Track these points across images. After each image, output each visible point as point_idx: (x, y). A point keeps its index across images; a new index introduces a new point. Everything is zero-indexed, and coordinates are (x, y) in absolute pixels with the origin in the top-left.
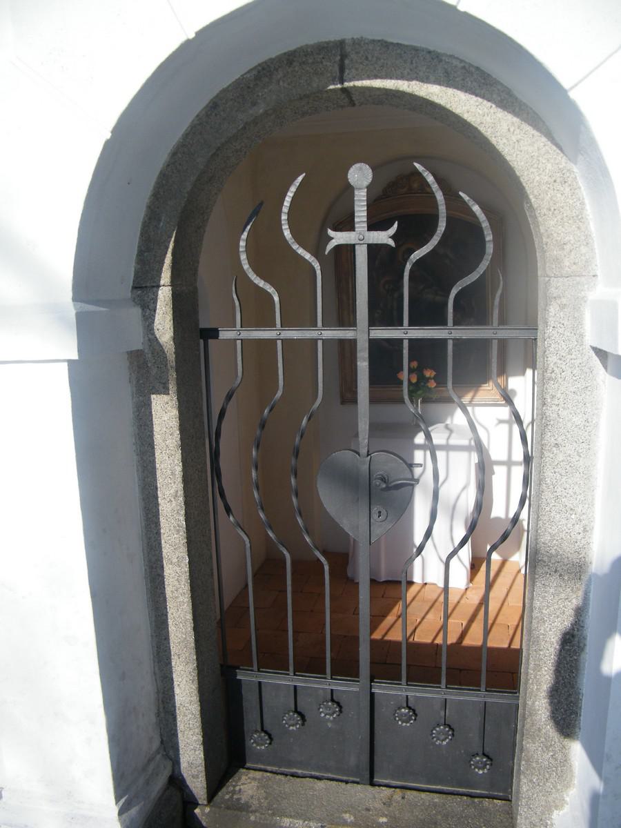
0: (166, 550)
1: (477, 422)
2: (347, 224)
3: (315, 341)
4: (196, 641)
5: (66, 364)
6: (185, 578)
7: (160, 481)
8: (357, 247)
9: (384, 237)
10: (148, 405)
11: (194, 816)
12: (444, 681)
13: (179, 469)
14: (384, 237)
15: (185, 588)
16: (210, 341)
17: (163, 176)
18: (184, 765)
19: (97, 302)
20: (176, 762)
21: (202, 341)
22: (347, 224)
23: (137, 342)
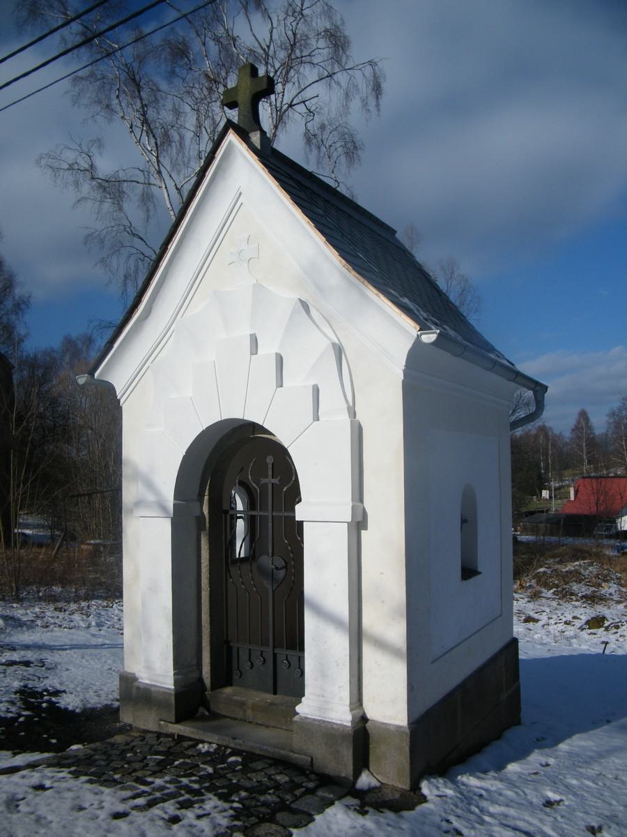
0: (203, 585)
1: (295, 188)
2: (266, 477)
3: (282, 516)
4: (210, 621)
5: (346, 524)
6: (208, 595)
7: (202, 561)
8: (304, 523)
9: (275, 481)
10: (200, 534)
11: (205, 695)
12: (298, 648)
13: (208, 557)
14: (275, 481)
15: (208, 600)
16: (363, 532)
17: (207, 461)
18: (204, 673)
19: (179, 500)
20: (201, 672)
21: (224, 515)
22: (266, 477)
23: (198, 513)
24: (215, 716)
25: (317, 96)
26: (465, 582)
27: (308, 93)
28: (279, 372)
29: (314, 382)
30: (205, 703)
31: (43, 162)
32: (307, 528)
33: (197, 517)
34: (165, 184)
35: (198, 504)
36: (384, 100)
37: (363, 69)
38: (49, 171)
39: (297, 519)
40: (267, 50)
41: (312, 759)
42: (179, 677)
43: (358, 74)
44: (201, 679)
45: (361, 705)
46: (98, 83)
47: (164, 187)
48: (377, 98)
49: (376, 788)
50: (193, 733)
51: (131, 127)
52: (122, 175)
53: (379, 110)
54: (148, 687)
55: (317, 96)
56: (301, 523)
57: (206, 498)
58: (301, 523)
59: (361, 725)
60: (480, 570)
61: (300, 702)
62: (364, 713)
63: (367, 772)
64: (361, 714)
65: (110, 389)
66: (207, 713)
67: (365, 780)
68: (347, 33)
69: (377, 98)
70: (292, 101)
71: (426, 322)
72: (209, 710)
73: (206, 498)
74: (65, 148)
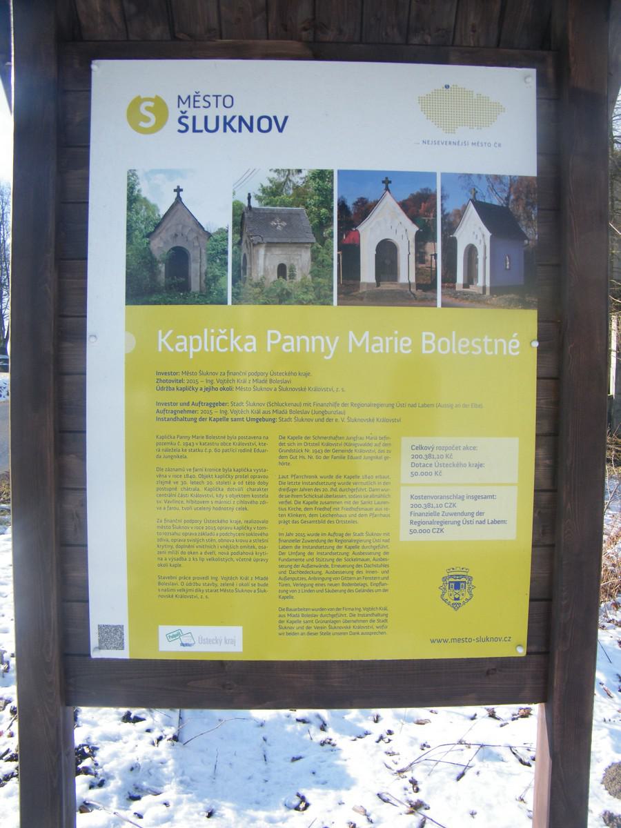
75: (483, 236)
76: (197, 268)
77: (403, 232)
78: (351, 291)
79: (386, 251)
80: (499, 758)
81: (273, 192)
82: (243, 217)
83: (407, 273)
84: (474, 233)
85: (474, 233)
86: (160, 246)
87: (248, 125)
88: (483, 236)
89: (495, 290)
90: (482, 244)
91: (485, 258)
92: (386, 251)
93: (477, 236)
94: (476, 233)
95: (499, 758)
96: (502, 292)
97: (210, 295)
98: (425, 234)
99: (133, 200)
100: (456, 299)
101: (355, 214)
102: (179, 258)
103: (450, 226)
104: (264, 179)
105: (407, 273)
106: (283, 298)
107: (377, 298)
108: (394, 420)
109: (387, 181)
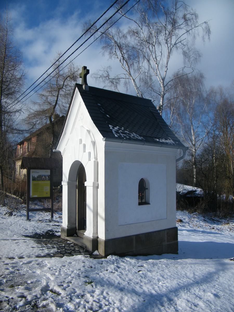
8: (87, 187)
23: (76, 184)
24: (78, 236)
25: (186, 39)
26: (139, 206)
27: (182, 38)
28: (84, 149)
29: (89, 151)
30: (76, 233)
31: (93, 76)
32: (87, 187)
33: (76, 185)
34: (132, 78)
35: (76, 182)
36: (211, 36)
37: (202, 26)
38: (95, 79)
39: (85, 185)
40: (165, 26)
41: (86, 246)
42: (69, 225)
43: (200, 28)
44: (76, 227)
45: (98, 234)
46: (110, 47)
47: (132, 79)
48: (209, 35)
49: (98, 255)
50: (69, 239)
51: (120, 61)
52: (119, 77)
53: (210, 40)
54: (64, 228)
55: (186, 39)
56: (86, 186)
57: (77, 180)
58: (86, 186)
59: (97, 238)
60: (150, 203)
61: (85, 232)
62: (98, 236)
63: (97, 251)
64: (97, 236)
65: (60, 152)
66: (76, 236)
67: (96, 252)
68: (197, 13)
69: (209, 35)
70: (175, 43)
71: (129, 133)
72: (77, 235)
73: (77, 180)
74: (99, 70)
75: (94, 143)
76: (35, 179)
77: (44, 177)
78: (42, 180)
79: (43, 178)
80: (19, 297)
81: (39, 176)
82: (37, 177)
83: (44, 179)
84: (81, 141)
85: (81, 141)
86: (34, 178)
87: (37, 173)
88: (94, 143)
89: (48, 180)
90: (93, 160)
91: (96, 187)
92: (43, 178)
93: (85, 146)
94: (83, 142)
95: (19, 297)
96: (49, 180)
97: (36, 180)
98: (45, 178)
99: (32, 176)
100: (46, 180)
101: (42, 177)
102: (34, 179)
103: (46, 177)
104: (38, 175)
105: (44, 179)
106: (39, 180)
107: (43, 180)
108: (160, 22)
109: (43, 175)
